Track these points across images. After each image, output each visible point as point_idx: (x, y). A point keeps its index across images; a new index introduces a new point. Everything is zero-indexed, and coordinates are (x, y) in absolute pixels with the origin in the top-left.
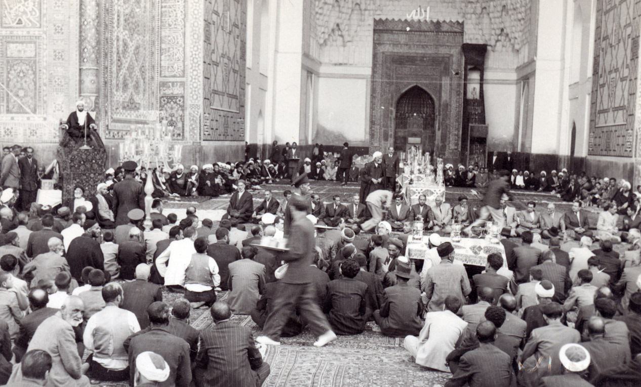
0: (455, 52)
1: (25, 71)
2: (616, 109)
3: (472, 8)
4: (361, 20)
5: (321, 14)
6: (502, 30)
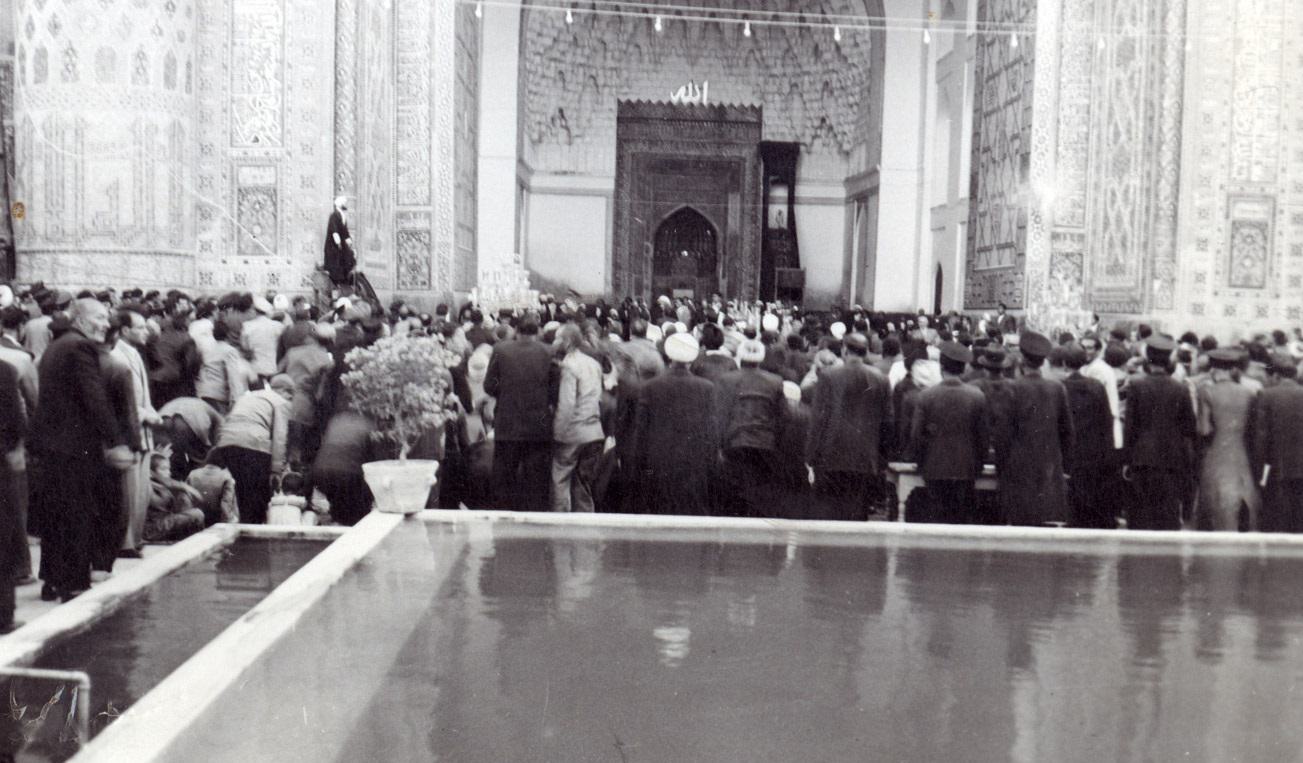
0: (748, 153)
2: (1001, 247)
3: (774, 83)
4: (597, 103)
5: (535, 94)
6: (823, 120)
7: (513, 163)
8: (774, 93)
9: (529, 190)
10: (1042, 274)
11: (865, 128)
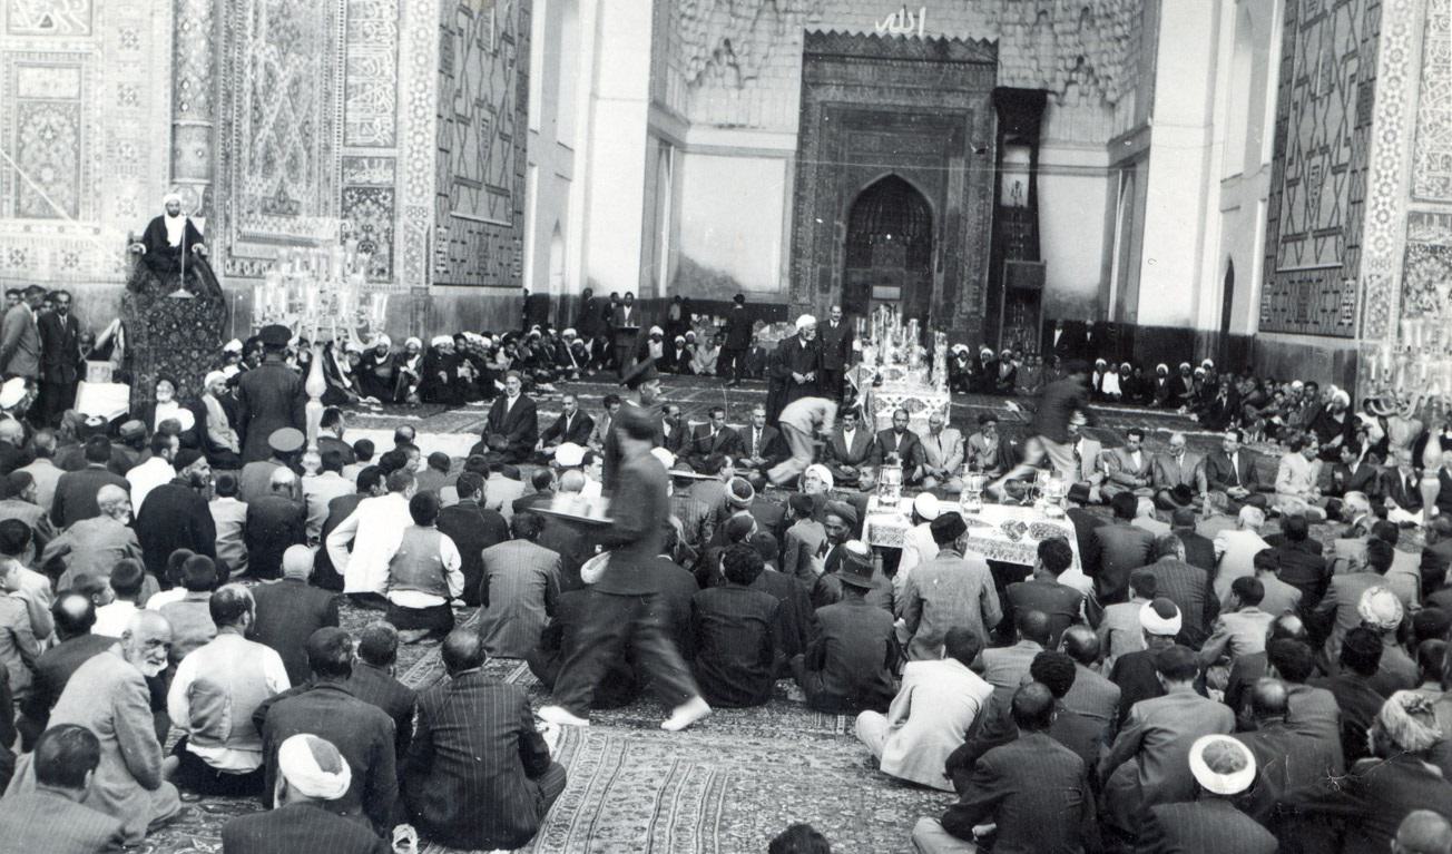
0: (978, 104)
1: (55, 126)
2: (1322, 234)
4: (777, 33)
5: (691, 18)
6: (1080, 60)
7: (644, 107)
8: (1015, 24)
9: (683, 148)
10: (1389, 280)
11: (1135, 69)
